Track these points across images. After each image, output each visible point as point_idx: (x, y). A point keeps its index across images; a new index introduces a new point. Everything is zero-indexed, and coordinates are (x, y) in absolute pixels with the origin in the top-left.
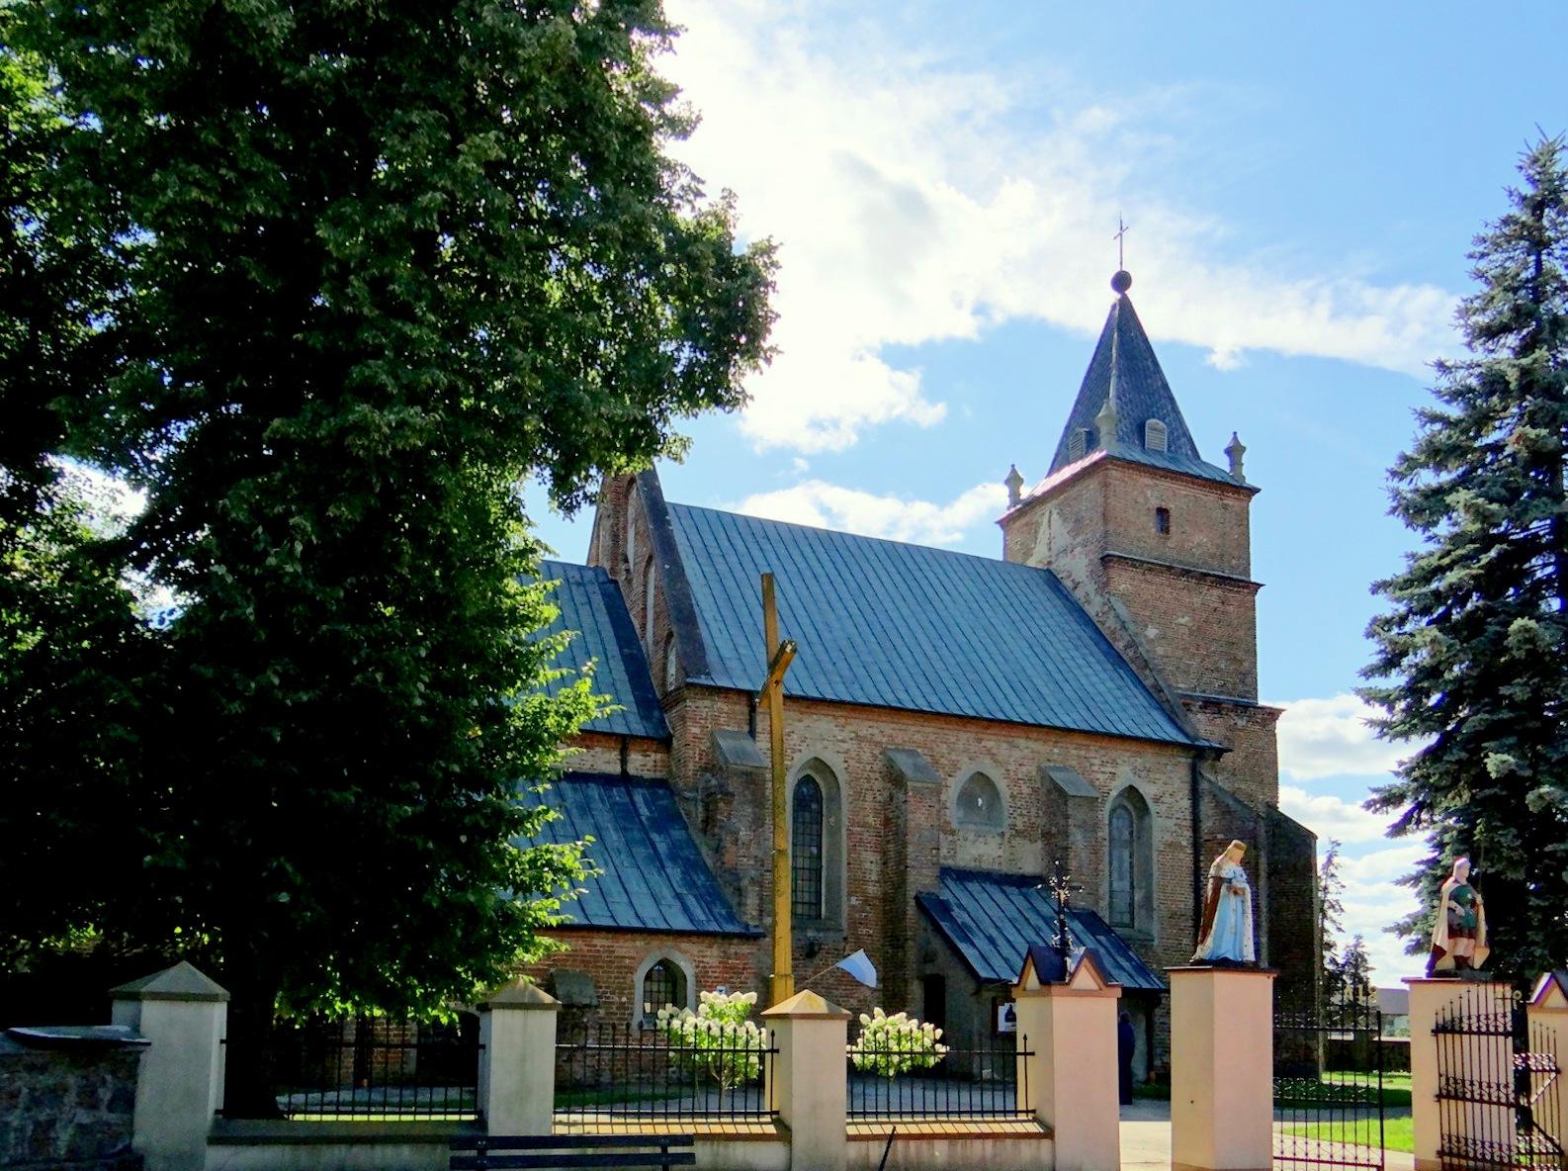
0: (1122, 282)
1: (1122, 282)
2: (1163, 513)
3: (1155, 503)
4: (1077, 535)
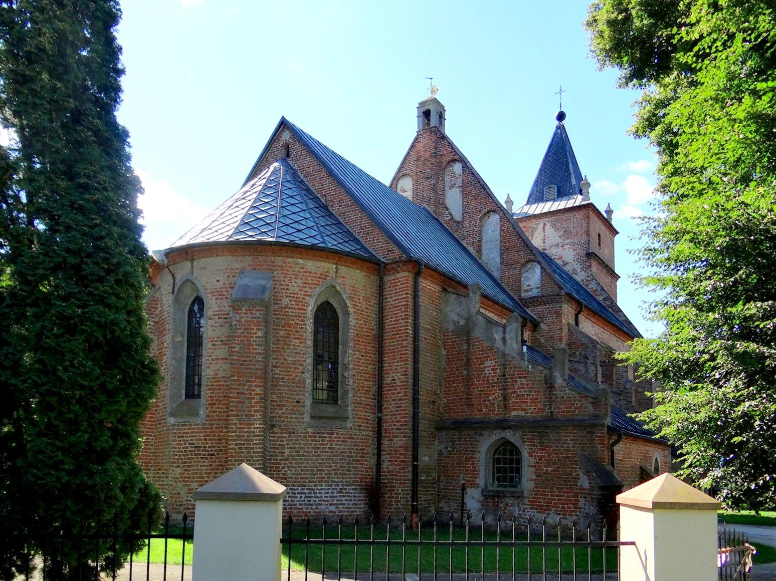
0: (561, 117)
1: (561, 117)
2: (599, 235)
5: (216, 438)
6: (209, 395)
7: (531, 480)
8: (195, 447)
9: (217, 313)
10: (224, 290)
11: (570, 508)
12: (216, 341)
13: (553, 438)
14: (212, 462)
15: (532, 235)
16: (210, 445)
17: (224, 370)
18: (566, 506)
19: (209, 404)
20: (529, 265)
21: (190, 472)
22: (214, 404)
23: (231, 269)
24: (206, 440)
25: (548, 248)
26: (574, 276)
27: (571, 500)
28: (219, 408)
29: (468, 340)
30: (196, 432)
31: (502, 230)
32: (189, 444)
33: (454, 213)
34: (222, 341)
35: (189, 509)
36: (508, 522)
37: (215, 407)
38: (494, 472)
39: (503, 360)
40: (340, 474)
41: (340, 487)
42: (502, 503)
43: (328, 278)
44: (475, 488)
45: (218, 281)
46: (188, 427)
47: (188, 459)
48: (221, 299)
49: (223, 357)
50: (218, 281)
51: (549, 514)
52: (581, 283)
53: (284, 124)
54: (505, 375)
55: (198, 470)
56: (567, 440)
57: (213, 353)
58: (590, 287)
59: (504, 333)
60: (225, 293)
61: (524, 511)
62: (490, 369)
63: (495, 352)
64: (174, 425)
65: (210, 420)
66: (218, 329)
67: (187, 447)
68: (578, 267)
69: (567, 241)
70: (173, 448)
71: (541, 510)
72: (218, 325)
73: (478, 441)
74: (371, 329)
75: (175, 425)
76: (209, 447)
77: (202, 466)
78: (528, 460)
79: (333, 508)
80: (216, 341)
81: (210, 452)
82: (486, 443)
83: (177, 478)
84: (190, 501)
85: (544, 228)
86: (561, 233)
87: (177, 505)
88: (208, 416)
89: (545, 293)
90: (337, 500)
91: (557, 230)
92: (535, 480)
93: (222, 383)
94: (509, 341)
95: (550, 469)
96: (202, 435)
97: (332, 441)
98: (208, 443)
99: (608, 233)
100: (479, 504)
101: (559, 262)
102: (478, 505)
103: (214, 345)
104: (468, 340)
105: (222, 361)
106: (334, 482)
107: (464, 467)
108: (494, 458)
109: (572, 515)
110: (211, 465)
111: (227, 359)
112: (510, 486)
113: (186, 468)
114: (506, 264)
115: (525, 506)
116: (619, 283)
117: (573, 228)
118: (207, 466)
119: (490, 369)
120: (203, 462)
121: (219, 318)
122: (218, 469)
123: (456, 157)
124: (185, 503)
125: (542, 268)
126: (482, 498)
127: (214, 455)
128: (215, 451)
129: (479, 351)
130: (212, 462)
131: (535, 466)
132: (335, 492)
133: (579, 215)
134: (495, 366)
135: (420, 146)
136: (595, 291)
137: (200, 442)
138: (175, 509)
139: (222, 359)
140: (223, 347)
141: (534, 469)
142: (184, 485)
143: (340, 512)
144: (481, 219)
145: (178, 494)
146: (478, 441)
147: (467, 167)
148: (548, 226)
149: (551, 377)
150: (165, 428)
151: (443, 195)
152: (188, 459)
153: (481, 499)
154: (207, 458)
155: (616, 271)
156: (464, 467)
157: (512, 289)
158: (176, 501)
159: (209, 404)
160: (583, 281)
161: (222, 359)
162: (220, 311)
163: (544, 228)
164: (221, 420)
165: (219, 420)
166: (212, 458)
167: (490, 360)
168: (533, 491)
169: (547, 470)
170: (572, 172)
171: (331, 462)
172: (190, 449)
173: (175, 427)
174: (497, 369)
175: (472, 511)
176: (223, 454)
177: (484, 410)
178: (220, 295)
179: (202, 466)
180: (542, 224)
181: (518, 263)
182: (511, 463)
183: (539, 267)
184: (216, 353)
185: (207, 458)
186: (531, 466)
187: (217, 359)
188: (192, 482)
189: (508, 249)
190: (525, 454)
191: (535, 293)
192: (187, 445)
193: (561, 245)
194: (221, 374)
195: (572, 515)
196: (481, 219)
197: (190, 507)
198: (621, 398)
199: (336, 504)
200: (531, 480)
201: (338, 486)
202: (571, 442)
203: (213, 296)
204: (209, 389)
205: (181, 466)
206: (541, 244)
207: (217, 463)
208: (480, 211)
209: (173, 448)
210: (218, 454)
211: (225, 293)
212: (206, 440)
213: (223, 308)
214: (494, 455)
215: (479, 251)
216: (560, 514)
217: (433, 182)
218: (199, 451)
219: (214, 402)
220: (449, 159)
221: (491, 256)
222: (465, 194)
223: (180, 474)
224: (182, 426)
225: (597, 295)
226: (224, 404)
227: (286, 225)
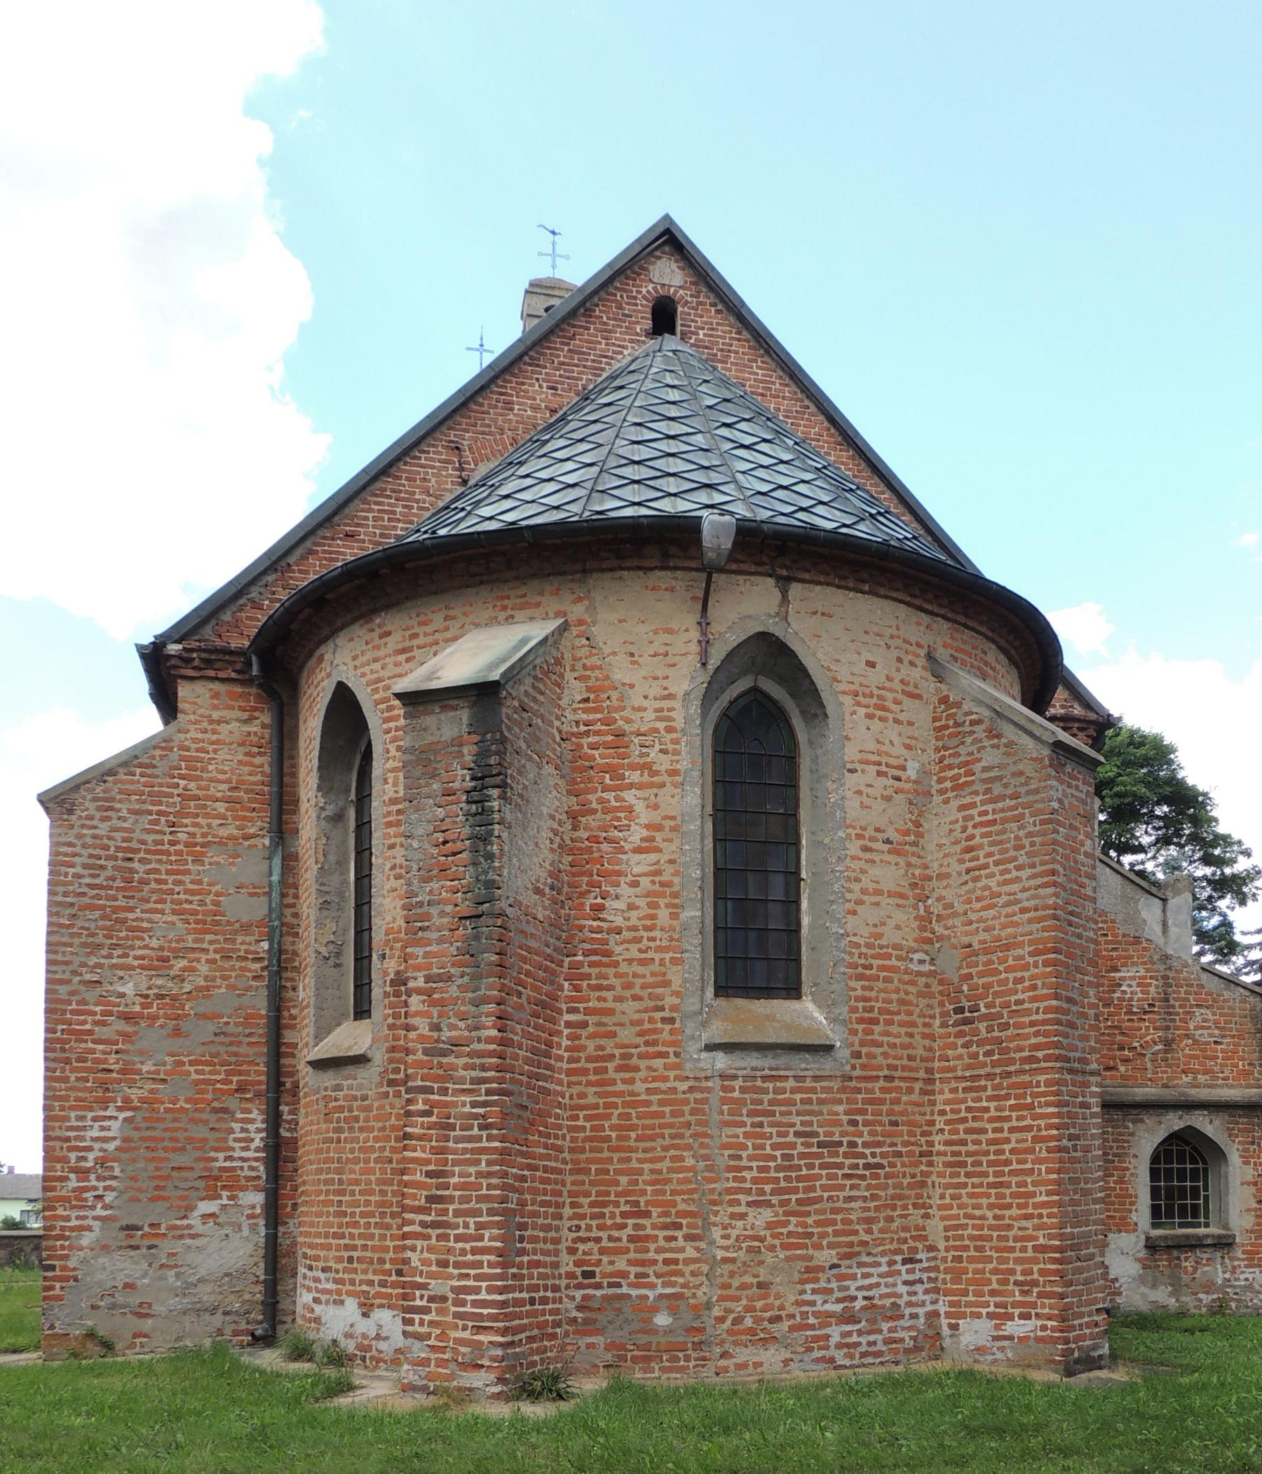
5: (885, 1119)
6: (859, 992)
7: (1248, 1210)
8: (820, 1145)
9: (875, 758)
10: (889, 696)
12: (873, 839)
14: (877, 1187)
16: (867, 1138)
17: (898, 927)
19: (860, 1021)
21: (810, 1221)
22: (875, 1021)
23: (905, 641)
24: (854, 1123)
28: (887, 1034)
30: (821, 1102)
32: (797, 1134)
34: (888, 841)
35: (812, 1327)
36: (1201, 1296)
37: (877, 1029)
39: (1162, 967)
42: (1186, 1259)
44: (1127, 1231)
45: (871, 664)
46: (791, 1083)
47: (799, 1179)
48: (881, 719)
49: (893, 887)
50: (871, 664)
53: (668, 240)
54: (1167, 1000)
55: (835, 1211)
57: (863, 871)
59: (1164, 911)
60: (894, 707)
62: (1134, 983)
63: (1144, 949)
64: (723, 1077)
65: (864, 1067)
66: (879, 805)
67: (792, 1146)
70: (725, 1146)
72: (876, 792)
73: (1132, 1134)
75: (735, 1077)
76: (865, 1145)
77: (850, 1199)
80: (873, 839)
81: (871, 1160)
83: (762, 1239)
84: (813, 1303)
87: (757, 1320)
88: (857, 1055)
92: (1255, 1210)
93: (894, 962)
94: (1173, 931)
96: (841, 1108)
97: (762, 1136)
98: (861, 1135)
100: (1138, 1266)
102: (1134, 1269)
103: (866, 849)
105: (892, 901)
110: (874, 1197)
111: (902, 896)
112: (1181, 1225)
113: (793, 1206)
118: (865, 1199)
119: (1134, 983)
120: (852, 1187)
121: (879, 774)
122: (894, 1208)
124: (791, 1309)
126: (1143, 1254)
127: (882, 1167)
128: (883, 1155)
129: (1107, 942)
130: (877, 1187)
131: (1255, 1184)
134: (1144, 978)
137: (837, 1130)
138: (751, 1331)
139: (891, 894)
140: (892, 858)
141: (1253, 1189)
142: (788, 1259)
145: (760, 1285)
146: (1132, 1134)
150: (683, 1086)
152: (799, 1179)
154: (863, 1177)
158: (749, 1309)
159: (860, 1021)
161: (891, 894)
162: (879, 753)
164: (895, 1068)
165: (890, 1067)
166: (877, 1176)
167: (1134, 964)
168: (1252, 1231)
172: (801, 1149)
173: (738, 1084)
175: (1122, 1281)
176: (904, 1165)
177: (1122, 1069)
178: (877, 707)
179: (850, 1199)
182: (1182, 1177)
184: (874, 872)
185: (863, 1177)
186: (1249, 1184)
187: (878, 892)
188: (818, 1247)
190: (1235, 1158)
192: (791, 1138)
194: (891, 936)
197: (812, 1321)
200: (1248, 1210)
203: (858, 704)
204: (860, 977)
205: (775, 1200)
207: (891, 1191)
209: (725, 1146)
210: (892, 1165)
211: (894, 707)
212: (854, 1123)
213: (886, 748)
218: (836, 1154)
219: (875, 1014)
223: (769, 1226)
224: (765, 1078)
226: (901, 1024)
227: (671, 495)
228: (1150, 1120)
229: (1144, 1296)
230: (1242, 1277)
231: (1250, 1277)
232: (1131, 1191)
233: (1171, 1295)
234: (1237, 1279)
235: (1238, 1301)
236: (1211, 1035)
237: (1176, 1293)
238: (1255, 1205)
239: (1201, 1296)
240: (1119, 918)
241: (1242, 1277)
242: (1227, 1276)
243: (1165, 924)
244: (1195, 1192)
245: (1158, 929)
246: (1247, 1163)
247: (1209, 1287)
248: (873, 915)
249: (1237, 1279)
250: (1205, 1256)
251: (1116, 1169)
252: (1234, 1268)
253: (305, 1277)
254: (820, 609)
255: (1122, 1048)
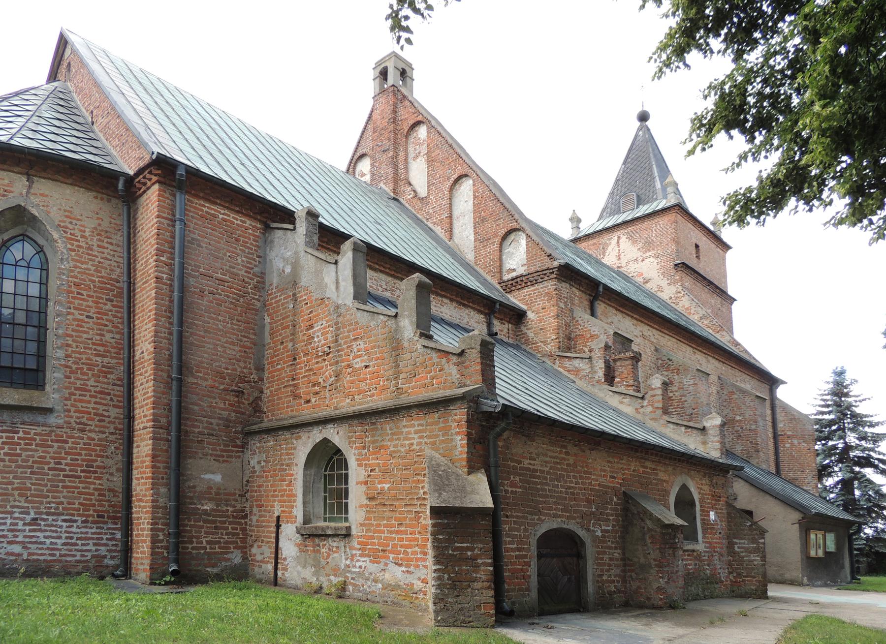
0: (643, 117)
1: (643, 117)
2: (697, 246)
3: (694, 241)
4: (649, 250)
7: (361, 506)
11: (415, 553)
13: (390, 432)
15: (604, 253)
18: (409, 550)
20: (512, 236)
25: (623, 264)
26: (659, 294)
27: (416, 540)
29: (294, 295)
31: (475, 197)
33: (419, 190)
36: (332, 578)
38: (325, 497)
40: (32, 496)
41: (32, 515)
43: (11, 195)
51: (386, 564)
52: (669, 302)
54: (337, 341)
56: (409, 433)
58: (680, 304)
59: (337, 272)
61: (352, 560)
68: (664, 283)
69: (648, 254)
71: (375, 558)
74: (113, 280)
78: (356, 473)
79: (17, 549)
82: (303, 446)
85: (618, 242)
86: (640, 245)
89: (533, 270)
90: (25, 537)
91: (634, 242)
92: (366, 506)
95: (387, 486)
99: (713, 246)
101: (640, 280)
104: (294, 295)
106: (18, 507)
107: (280, 491)
108: (325, 476)
109: (418, 566)
114: (481, 240)
115: (354, 552)
116: (735, 307)
117: (656, 237)
123: (420, 118)
125: (528, 236)
131: (366, 483)
132: (21, 523)
133: (663, 222)
135: (376, 116)
136: (687, 309)
141: (364, 488)
143: (30, 554)
144: (451, 189)
146: (295, 449)
147: (437, 131)
148: (624, 239)
149: (397, 330)
151: (407, 168)
153: (298, 541)
155: (730, 292)
156: (280, 491)
157: (490, 271)
160: (671, 298)
163: (618, 242)
169: (382, 489)
170: (656, 174)
171: (11, 476)
174: (327, 332)
175: (289, 560)
180: (616, 238)
181: (496, 235)
183: (524, 236)
186: (361, 483)
189: (483, 221)
190: (352, 463)
191: (521, 271)
193: (640, 259)
195: (418, 566)
196: (451, 189)
198: (645, 403)
199: (22, 542)
200: (361, 506)
201: (28, 513)
202: (416, 436)
206: (615, 260)
208: (449, 179)
214: (325, 471)
215: (450, 231)
216: (401, 565)
217: (391, 153)
220: (411, 122)
221: (465, 234)
222: (430, 162)
225: (690, 313)
228: (304, 435)
229: (299, 573)
230: (358, 564)
231: (363, 564)
232: (294, 492)
233: (314, 574)
234: (354, 566)
235: (354, 585)
236: (362, 361)
237: (316, 574)
238: (365, 502)
239: (332, 578)
240: (312, 289)
241: (358, 564)
242: (348, 562)
243: (337, 282)
244: (291, 490)
245: (333, 287)
246: (360, 465)
247: (336, 571)
248: (752, 404)
249: (354, 566)
250: (335, 544)
251: (288, 475)
252: (353, 556)
253: (722, 548)
254: (641, 263)
255: (314, 385)
